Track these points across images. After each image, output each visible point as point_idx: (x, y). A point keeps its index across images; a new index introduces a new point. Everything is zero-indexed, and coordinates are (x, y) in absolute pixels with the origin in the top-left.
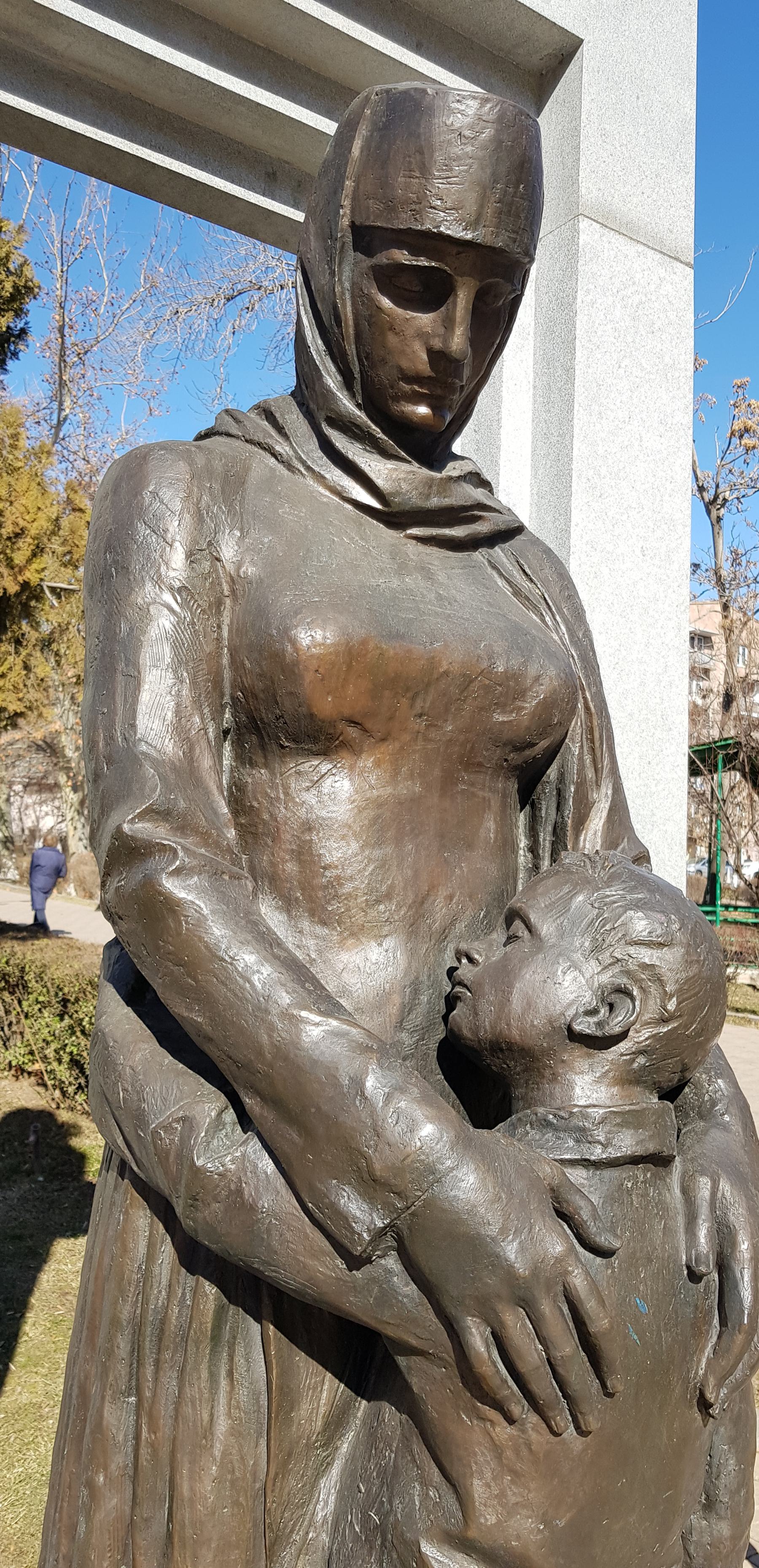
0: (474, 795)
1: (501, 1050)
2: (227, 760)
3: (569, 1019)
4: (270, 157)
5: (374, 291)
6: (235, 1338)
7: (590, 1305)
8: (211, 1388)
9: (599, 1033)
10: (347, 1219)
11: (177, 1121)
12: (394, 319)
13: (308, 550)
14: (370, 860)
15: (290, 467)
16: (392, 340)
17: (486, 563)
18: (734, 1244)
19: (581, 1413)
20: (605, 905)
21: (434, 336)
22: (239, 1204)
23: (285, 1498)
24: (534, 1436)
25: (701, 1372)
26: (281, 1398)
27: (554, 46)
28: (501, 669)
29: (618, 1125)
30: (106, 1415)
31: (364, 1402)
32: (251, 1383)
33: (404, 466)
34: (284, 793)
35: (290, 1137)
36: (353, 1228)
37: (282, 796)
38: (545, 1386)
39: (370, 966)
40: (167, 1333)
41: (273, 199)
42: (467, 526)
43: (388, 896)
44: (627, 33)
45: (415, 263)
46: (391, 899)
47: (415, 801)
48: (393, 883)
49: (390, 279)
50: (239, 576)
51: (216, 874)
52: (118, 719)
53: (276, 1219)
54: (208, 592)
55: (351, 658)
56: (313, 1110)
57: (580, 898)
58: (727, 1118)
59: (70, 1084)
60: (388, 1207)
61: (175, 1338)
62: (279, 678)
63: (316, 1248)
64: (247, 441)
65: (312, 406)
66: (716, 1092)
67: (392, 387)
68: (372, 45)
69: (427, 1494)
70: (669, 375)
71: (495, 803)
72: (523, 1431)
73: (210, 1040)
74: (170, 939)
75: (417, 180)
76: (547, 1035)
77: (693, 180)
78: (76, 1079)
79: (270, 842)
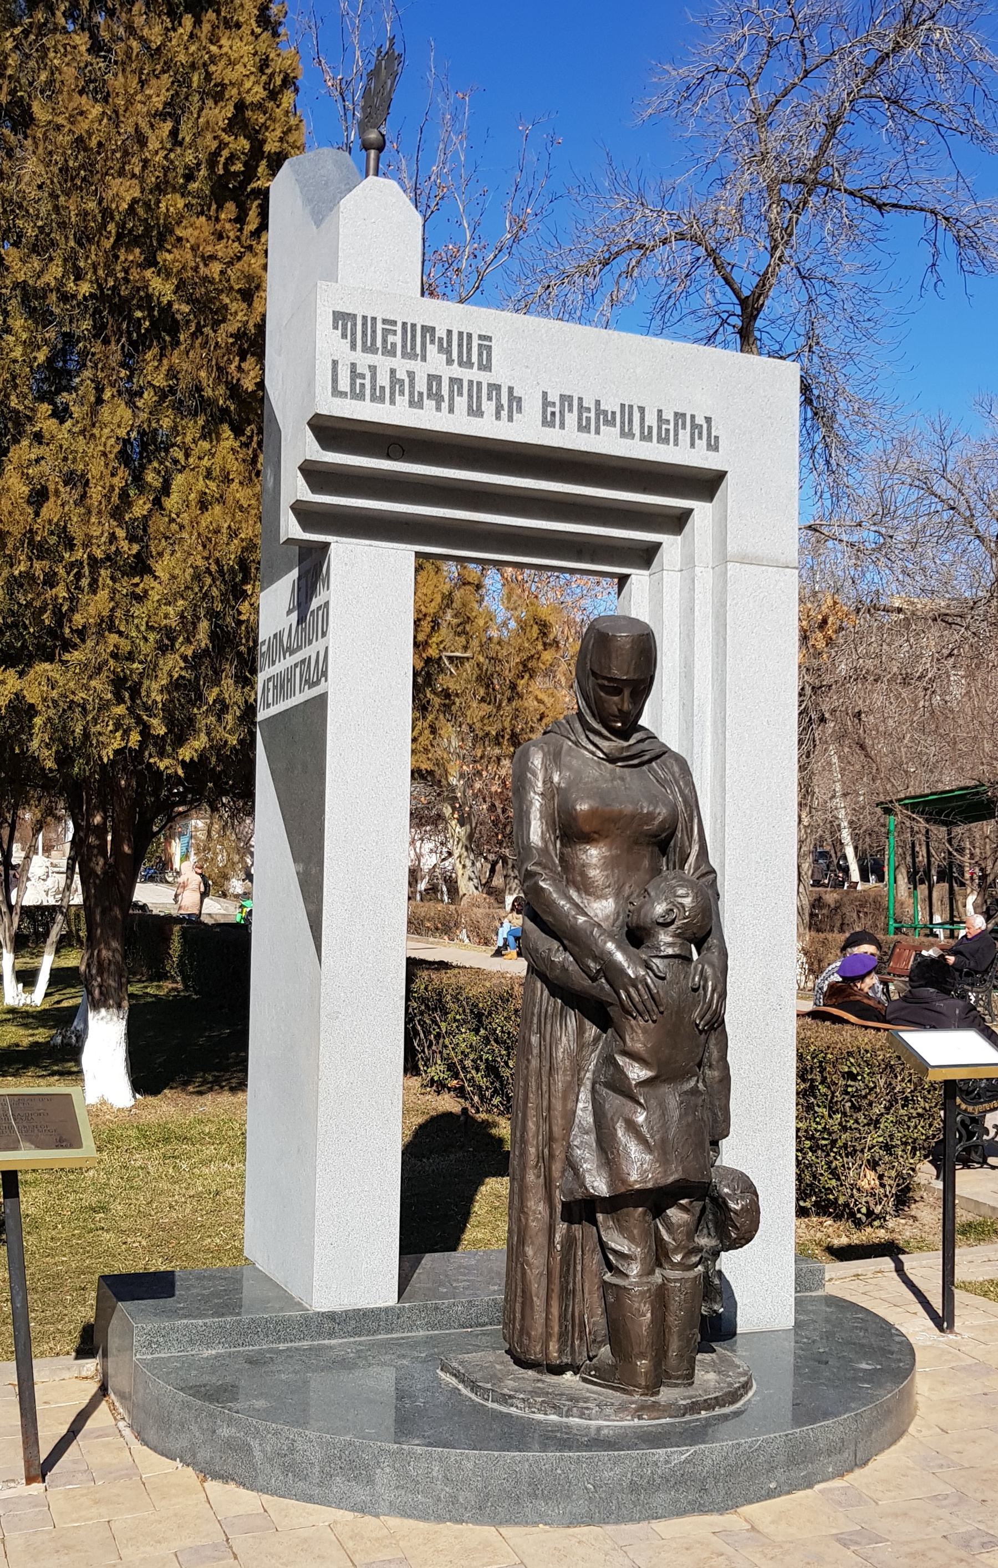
2: (558, 845)
22: (564, 969)
26: (581, 1031)
38: (641, 1007)
39: (603, 908)
47: (618, 856)
49: (602, 687)
51: (554, 880)
54: (551, 792)
55: (593, 813)
59: (487, 1088)
71: (648, 856)
78: (492, 1083)
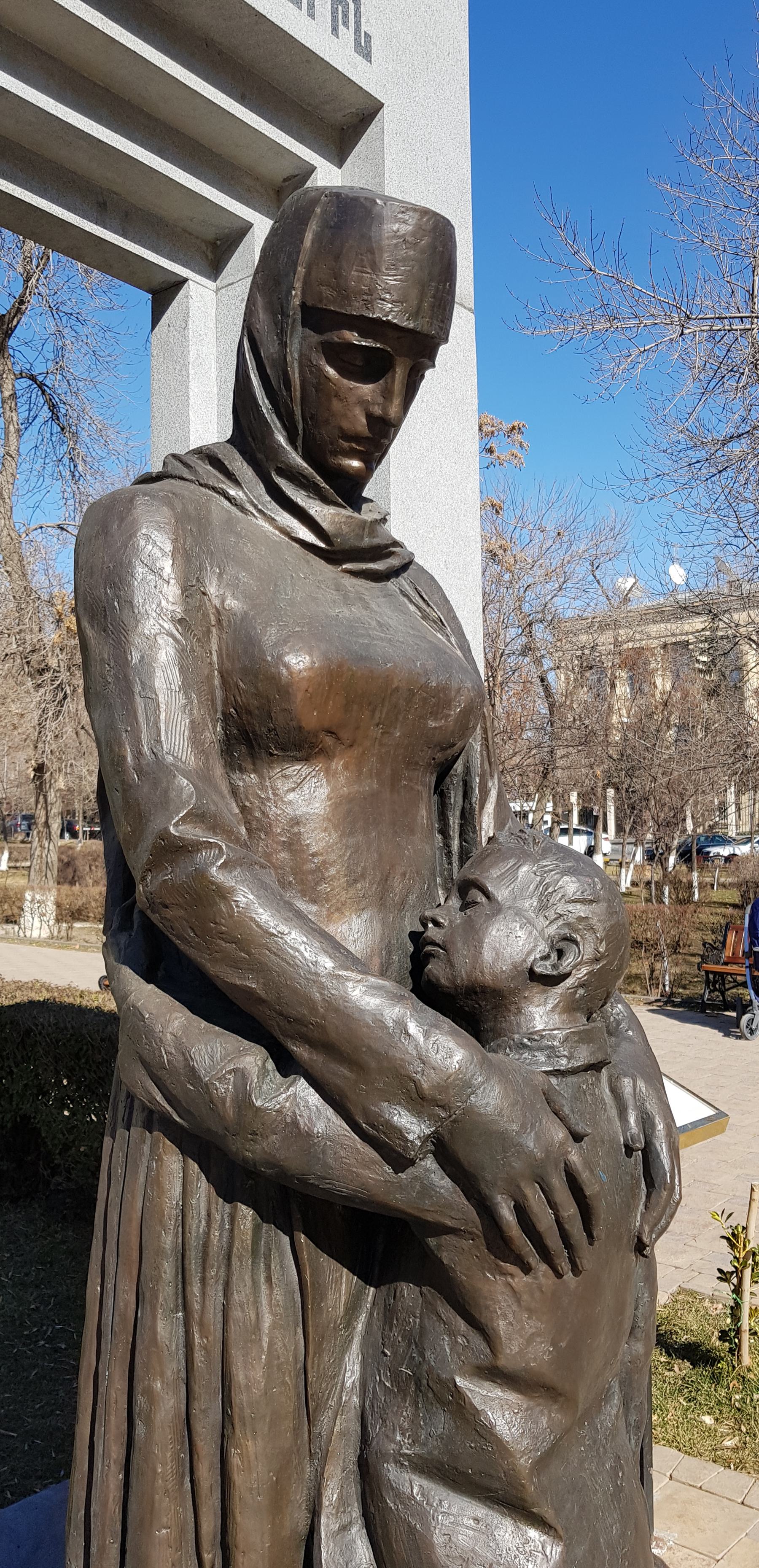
0: (412, 788)
1: (476, 993)
3: (529, 964)
4: (101, 187)
5: (323, 362)
6: (270, 1250)
7: (584, 1176)
8: (255, 1294)
9: (555, 973)
10: (400, 1131)
11: (230, 1072)
12: (340, 388)
13: (276, 585)
14: (347, 847)
15: (242, 509)
16: (336, 405)
17: (398, 591)
18: (653, 1126)
19: (579, 1258)
20: (545, 872)
21: (373, 404)
23: (322, 1371)
24: (543, 1280)
25: (637, 1224)
26: (307, 1295)
27: (357, 107)
28: (434, 684)
29: (576, 1041)
30: (159, 1330)
31: (372, 1289)
32: (287, 1285)
33: (343, 512)
34: (273, 794)
35: (339, 1074)
36: (406, 1138)
37: (271, 796)
38: (554, 1242)
40: (211, 1254)
41: (105, 228)
42: (372, 558)
43: (363, 876)
44: (417, 99)
45: (364, 344)
46: (365, 879)
48: (365, 865)
49: (338, 354)
50: (224, 608)
52: (144, 737)
53: (330, 1141)
54: (194, 619)
56: (364, 1049)
57: (525, 869)
58: (630, 1033)
60: (432, 1117)
61: (218, 1257)
62: (275, 697)
63: (367, 1160)
64: (201, 485)
65: (260, 456)
66: (618, 1014)
67: (332, 444)
68: (205, 95)
69: (457, 1342)
70: (460, 409)
72: (536, 1278)
73: (261, 1001)
74: (223, 921)
75: (369, 276)
76: (513, 978)
77: (471, 234)
79: (263, 836)
